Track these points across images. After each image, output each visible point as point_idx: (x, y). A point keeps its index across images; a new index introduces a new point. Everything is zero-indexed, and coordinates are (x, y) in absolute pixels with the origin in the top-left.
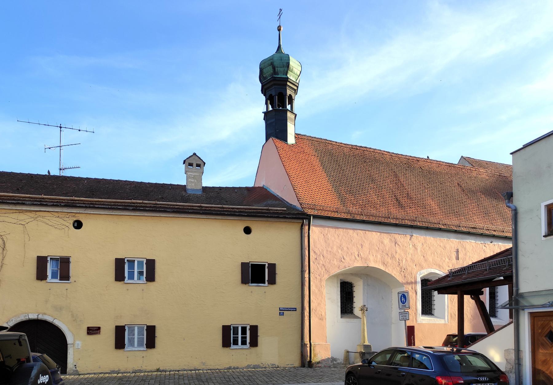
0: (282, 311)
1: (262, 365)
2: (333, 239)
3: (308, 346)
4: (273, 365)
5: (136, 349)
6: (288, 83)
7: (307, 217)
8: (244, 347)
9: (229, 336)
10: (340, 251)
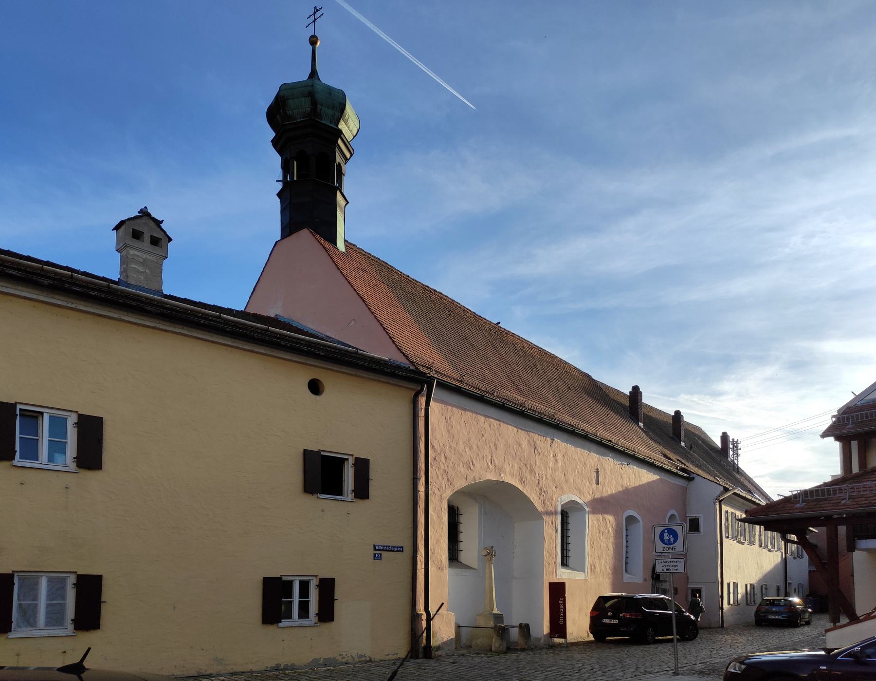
0: (379, 552)
1: (340, 659)
2: (458, 428)
3: (424, 617)
4: (361, 656)
5: (45, 633)
6: (340, 142)
7: (429, 381)
8: (305, 622)
9: (276, 600)
10: (467, 450)
